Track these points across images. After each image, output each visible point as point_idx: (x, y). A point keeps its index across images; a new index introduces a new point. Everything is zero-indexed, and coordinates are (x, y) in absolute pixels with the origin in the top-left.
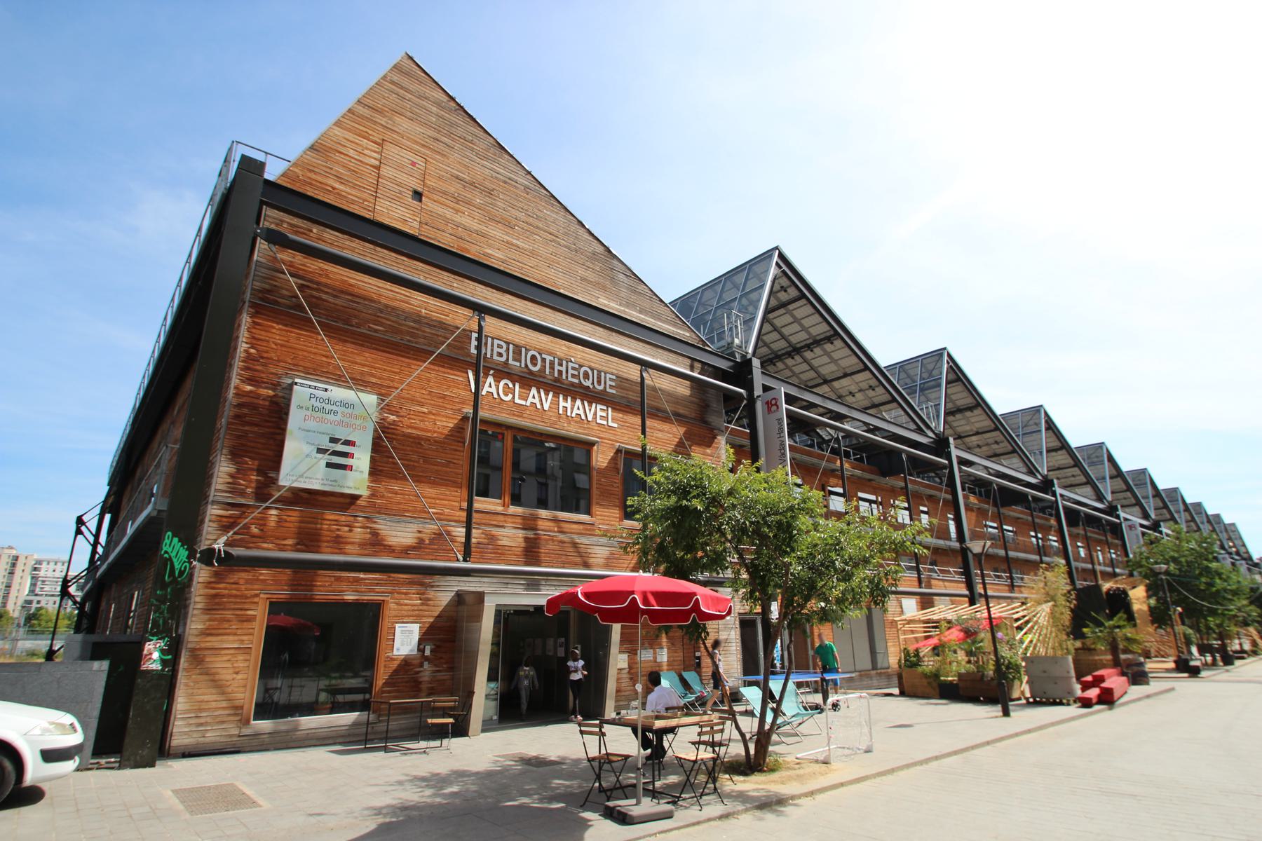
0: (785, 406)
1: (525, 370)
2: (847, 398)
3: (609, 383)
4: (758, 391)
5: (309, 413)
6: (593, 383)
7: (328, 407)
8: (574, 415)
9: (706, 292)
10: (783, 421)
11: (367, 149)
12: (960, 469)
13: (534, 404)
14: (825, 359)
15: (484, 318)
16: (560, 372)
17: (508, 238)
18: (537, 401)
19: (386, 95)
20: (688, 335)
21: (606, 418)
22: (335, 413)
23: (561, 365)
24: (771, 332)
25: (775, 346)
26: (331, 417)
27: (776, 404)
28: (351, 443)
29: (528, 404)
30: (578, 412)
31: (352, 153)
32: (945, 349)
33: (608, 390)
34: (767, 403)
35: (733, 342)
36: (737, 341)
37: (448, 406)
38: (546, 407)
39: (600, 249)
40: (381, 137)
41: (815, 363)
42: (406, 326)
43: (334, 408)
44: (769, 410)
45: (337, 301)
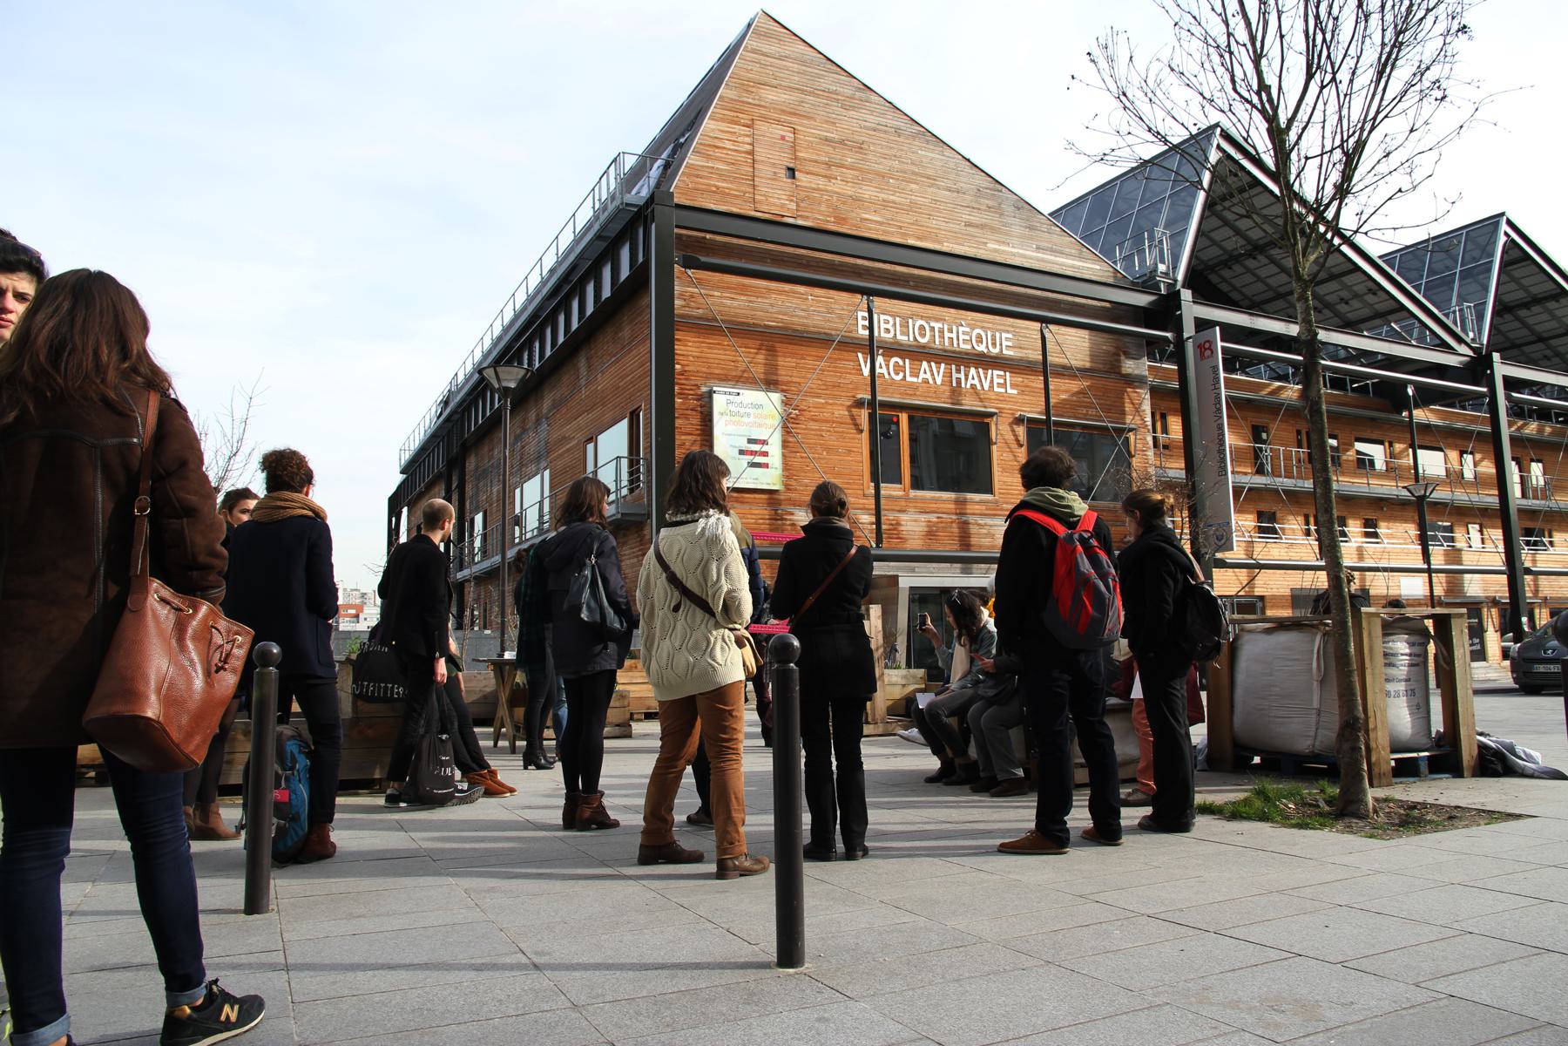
0: (1220, 344)
1: (915, 343)
2: (1338, 307)
3: (1005, 343)
4: (1189, 330)
5: (728, 418)
6: (987, 347)
7: (742, 410)
8: (968, 386)
9: (1126, 184)
10: (1218, 369)
11: (741, 135)
12: (1508, 398)
13: (926, 381)
14: (1545, 317)
15: (873, 301)
16: (958, 371)
17: (883, 195)
18: (928, 376)
19: (750, 68)
20: (1098, 267)
21: (1004, 385)
22: (748, 415)
23: (951, 331)
24: (1220, 227)
25: (1229, 245)
26: (745, 419)
27: (1210, 349)
28: (764, 442)
29: (920, 380)
30: (973, 382)
31: (728, 145)
32: (1503, 214)
33: (1005, 352)
34: (1200, 346)
35: (1155, 269)
36: (1162, 268)
37: (843, 394)
38: (939, 381)
39: (986, 182)
40: (750, 117)
41: (1530, 321)
42: (797, 316)
43: (747, 410)
44: (1202, 356)
45: (735, 303)
